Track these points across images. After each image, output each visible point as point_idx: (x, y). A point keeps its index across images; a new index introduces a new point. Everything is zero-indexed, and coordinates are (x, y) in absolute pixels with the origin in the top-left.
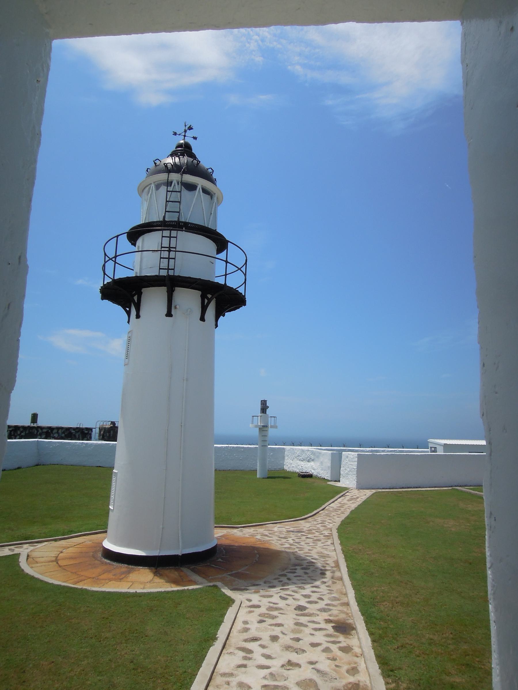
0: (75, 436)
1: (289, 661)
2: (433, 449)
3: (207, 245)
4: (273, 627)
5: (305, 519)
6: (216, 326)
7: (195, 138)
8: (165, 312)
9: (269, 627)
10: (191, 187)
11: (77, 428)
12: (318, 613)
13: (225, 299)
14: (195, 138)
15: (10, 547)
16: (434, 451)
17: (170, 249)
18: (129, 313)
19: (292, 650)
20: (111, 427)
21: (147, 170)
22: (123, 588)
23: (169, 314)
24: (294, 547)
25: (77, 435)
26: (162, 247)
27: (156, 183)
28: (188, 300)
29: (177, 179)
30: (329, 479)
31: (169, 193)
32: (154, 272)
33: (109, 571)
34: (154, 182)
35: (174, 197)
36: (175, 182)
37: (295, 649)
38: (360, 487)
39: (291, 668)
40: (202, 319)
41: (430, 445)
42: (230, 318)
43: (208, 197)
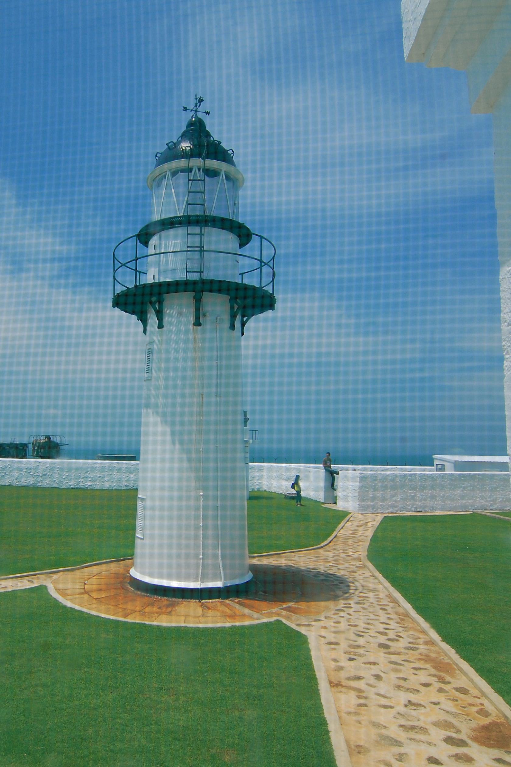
0: (9, 453)
1: (409, 701)
2: (440, 467)
3: (226, 240)
4: (369, 666)
5: (322, 547)
6: (243, 334)
7: (208, 113)
8: (192, 319)
9: (363, 665)
10: (212, 173)
11: (11, 443)
12: (406, 651)
13: (250, 301)
14: (208, 113)
15: (27, 578)
16: (440, 470)
17: (201, 249)
18: (144, 320)
19: (404, 689)
20: (46, 442)
21: (156, 156)
22: (164, 621)
23: (197, 323)
24: (332, 579)
25: (11, 451)
26: (188, 247)
27: (173, 170)
28: (217, 306)
29: (199, 165)
30: (322, 501)
31: (190, 182)
32: (181, 276)
33: (152, 605)
34: (170, 170)
35: (199, 186)
36: (195, 169)
37: (408, 689)
38: (363, 508)
39: (416, 708)
40: (232, 327)
41: (436, 462)
42: (257, 324)
43: (231, 184)
